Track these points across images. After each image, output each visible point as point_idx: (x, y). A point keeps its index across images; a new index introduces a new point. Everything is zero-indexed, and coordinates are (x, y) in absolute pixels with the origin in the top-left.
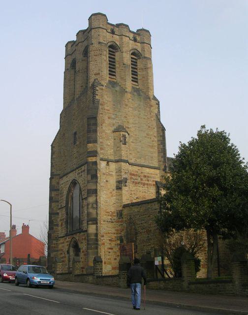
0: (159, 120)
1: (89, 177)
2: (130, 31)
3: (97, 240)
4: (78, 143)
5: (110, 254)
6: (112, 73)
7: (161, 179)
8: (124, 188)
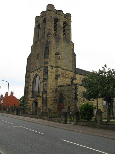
0: (73, 51)
1: (45, 72)
3: (46, 100)
4: (39, 58)
6: (55, 30)
7: (73, 76)
8: (58, 78)
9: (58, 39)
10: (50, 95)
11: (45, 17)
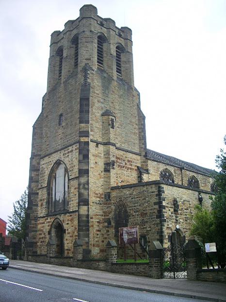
0: (140, 109)
1: (81, 157)
2: (116, 27)
3: (88, 222)
4: (64, 124)
5: (98, 236)
6: (100, 61)
7: (142, 165)
8: (112, 170)
9: (107, 81)
10: (95, 210)
11: (75, 32)
